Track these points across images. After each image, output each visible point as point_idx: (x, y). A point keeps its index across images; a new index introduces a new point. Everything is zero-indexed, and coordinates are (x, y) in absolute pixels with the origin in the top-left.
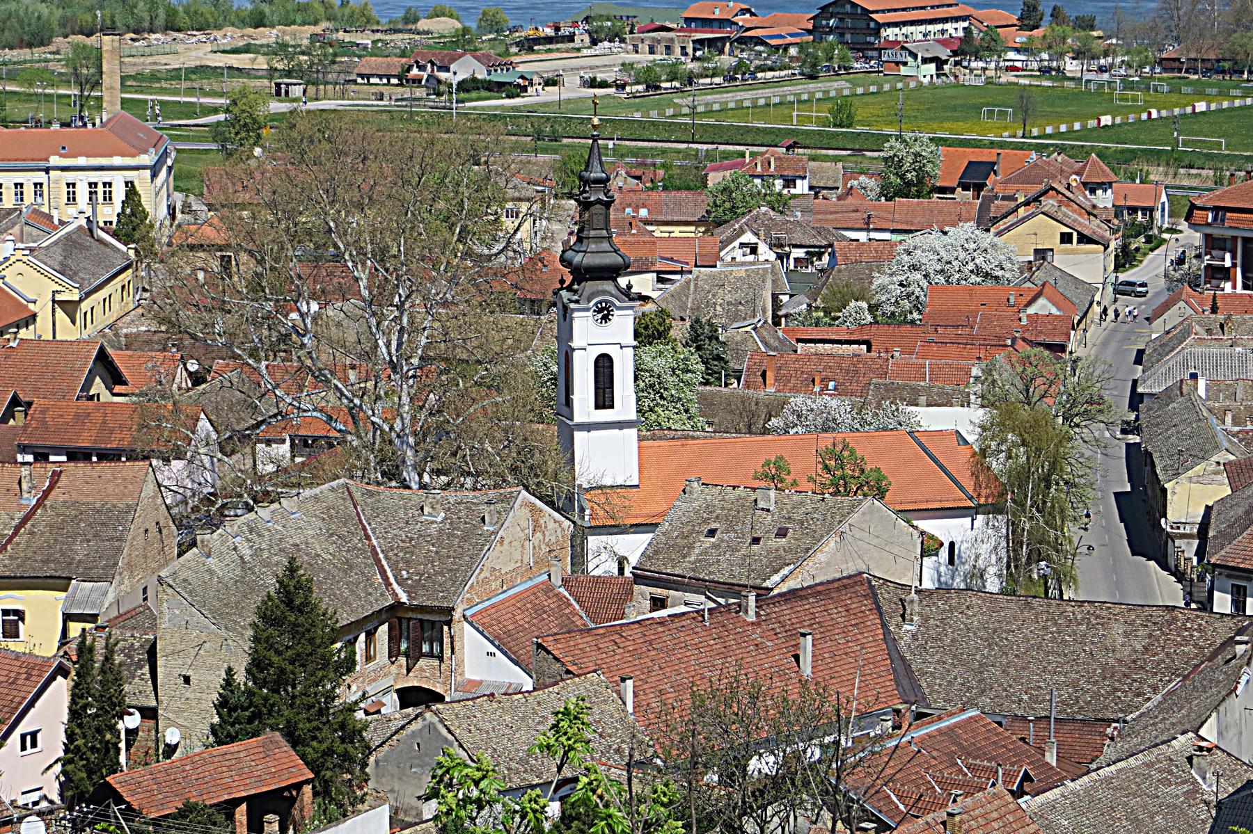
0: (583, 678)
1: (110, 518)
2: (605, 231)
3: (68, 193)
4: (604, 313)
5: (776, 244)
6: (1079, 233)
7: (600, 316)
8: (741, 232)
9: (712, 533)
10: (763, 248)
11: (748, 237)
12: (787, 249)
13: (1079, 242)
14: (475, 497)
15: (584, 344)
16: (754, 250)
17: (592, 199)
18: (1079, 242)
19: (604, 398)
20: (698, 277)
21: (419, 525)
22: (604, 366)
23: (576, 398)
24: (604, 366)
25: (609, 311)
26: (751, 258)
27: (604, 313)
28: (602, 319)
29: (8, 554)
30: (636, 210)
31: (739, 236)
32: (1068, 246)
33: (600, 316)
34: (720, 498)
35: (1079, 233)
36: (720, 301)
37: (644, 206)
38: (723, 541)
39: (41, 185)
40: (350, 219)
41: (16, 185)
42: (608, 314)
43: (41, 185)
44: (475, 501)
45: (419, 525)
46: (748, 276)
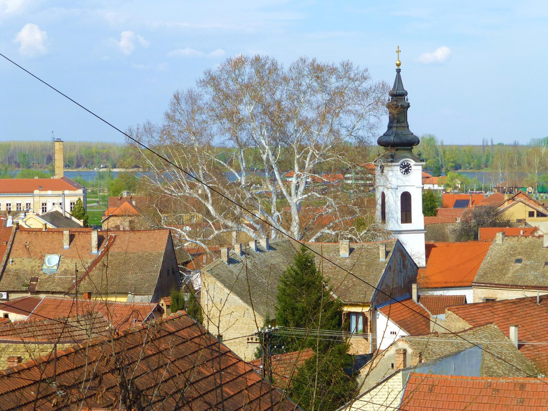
0: (485, 326)
1: (149, 260)
3: (43, 208)
4: (406, 169)
6: (537, 212)
7: (404, 170)
9: (519, 261)
13: (538, 216)
14: (368, 246)
18: (538, 216)
21: (338, 260)
22: (406, 198)
24: (406, 198)
25: (409, 167)
28: (405, 172)
29: (86, 281)
32: (532, 218)
33: (404, 170)
34: (519, 243)
35: (537, 212)
38: (526, 265)
39: (30, 204)
40: (278, 96)
41: (17, 204)
42: (408, 169)
43: (30, 204)
44: (369, 247)
45: (338, 260)
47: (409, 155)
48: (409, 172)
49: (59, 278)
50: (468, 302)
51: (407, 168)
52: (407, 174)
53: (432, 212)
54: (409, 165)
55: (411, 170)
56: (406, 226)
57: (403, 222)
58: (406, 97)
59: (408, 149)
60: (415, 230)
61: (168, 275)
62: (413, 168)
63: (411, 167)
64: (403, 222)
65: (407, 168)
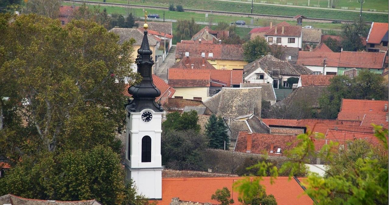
2: (149, 78)
5: (273, 74)
7: (145, 118)
8: (256, 68)
10: (266, 76)
11: (259, 70)
12: (280, 76)
15: (137, 131)
16: (262, 77)
17: (143, 63)
19: (146, 156)
20: (225, 92)
22: (147, 142)
23: (133, 156)
24: (147, 142)
25: (150, 116)
26: (261, 81)
27: (147, 117)
28: (146, 119)
30: (207, 53)
31: (255, 69)
33: (145, 118)
36: (235, 105)
37: (211, 52)
42: (149, 117)
46: (250, 92)
47: (151, 105)
48: (150, 120)
49: (36, 129)
50: (161, 198)
51: (148, 116)
52: (148, 121)
53: (45, 84)
54: (150, 113)
55: (151, 118)
56: (146, 165)
57: (143, 161)
58: (151, 55)
59: (151, 100)
60: (153, 168)
61: (216, 65)
62: (154, 116)
63: (151, 115)
64: (143, 161)
65: (148, 116)
